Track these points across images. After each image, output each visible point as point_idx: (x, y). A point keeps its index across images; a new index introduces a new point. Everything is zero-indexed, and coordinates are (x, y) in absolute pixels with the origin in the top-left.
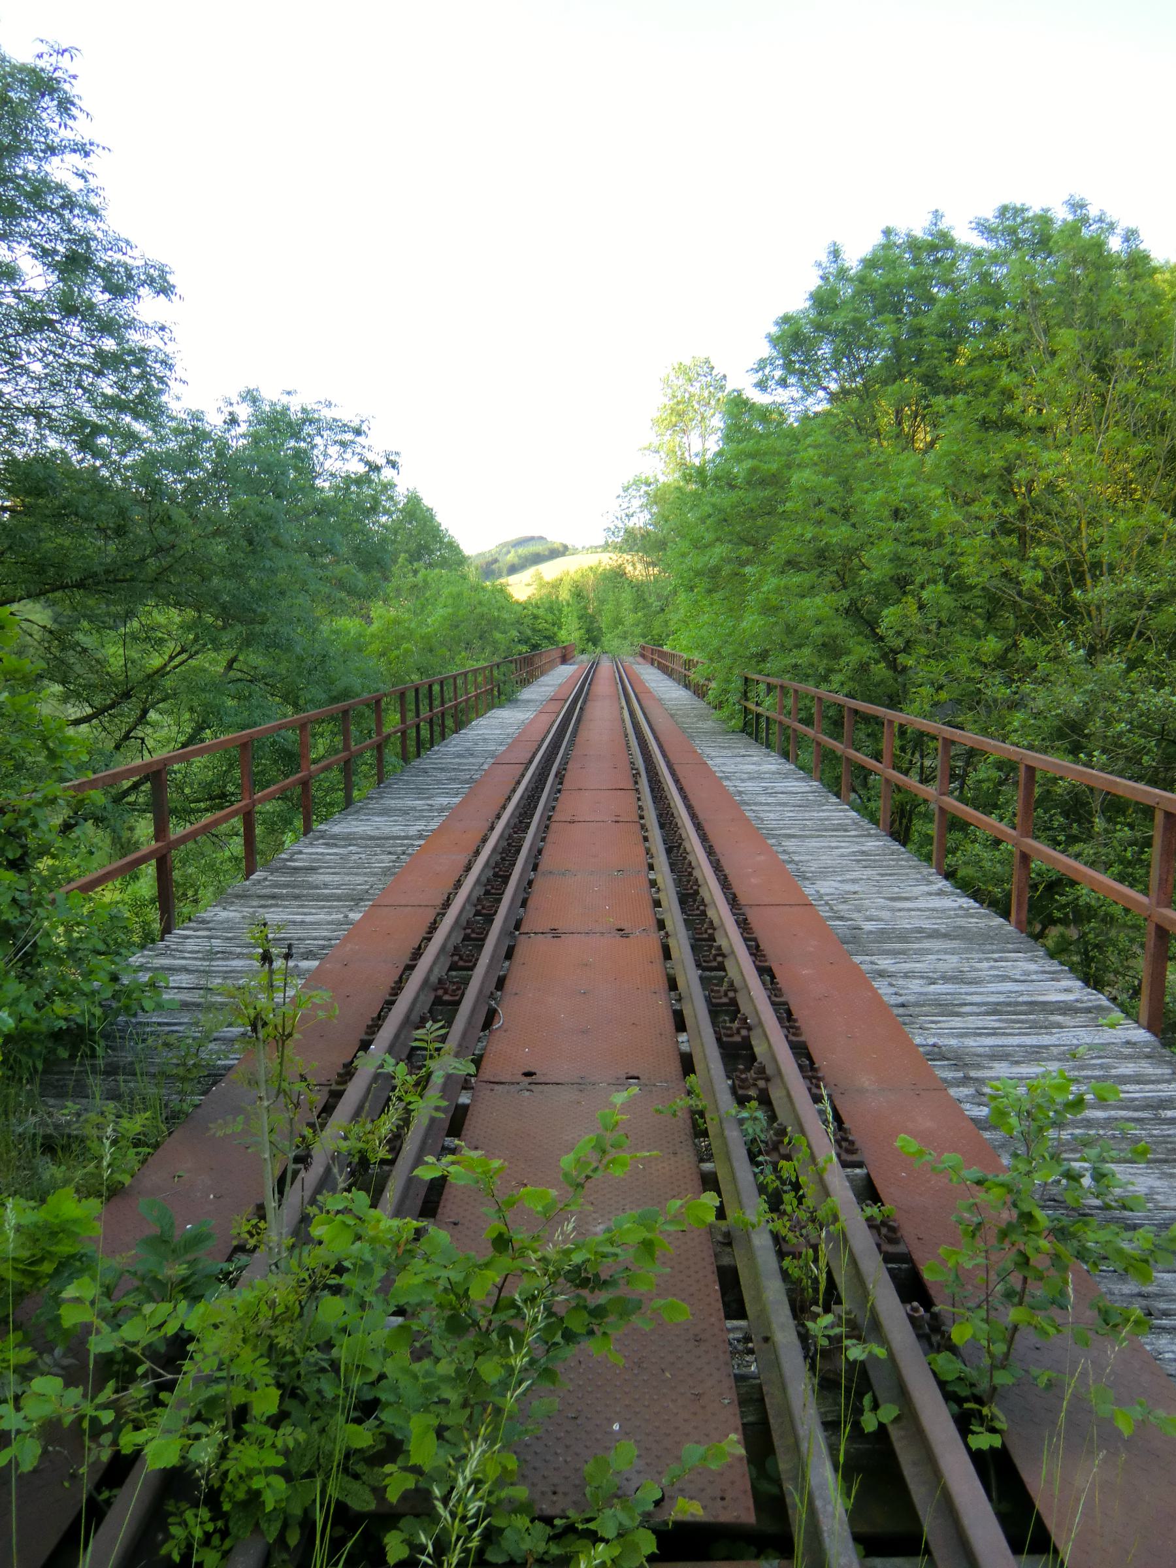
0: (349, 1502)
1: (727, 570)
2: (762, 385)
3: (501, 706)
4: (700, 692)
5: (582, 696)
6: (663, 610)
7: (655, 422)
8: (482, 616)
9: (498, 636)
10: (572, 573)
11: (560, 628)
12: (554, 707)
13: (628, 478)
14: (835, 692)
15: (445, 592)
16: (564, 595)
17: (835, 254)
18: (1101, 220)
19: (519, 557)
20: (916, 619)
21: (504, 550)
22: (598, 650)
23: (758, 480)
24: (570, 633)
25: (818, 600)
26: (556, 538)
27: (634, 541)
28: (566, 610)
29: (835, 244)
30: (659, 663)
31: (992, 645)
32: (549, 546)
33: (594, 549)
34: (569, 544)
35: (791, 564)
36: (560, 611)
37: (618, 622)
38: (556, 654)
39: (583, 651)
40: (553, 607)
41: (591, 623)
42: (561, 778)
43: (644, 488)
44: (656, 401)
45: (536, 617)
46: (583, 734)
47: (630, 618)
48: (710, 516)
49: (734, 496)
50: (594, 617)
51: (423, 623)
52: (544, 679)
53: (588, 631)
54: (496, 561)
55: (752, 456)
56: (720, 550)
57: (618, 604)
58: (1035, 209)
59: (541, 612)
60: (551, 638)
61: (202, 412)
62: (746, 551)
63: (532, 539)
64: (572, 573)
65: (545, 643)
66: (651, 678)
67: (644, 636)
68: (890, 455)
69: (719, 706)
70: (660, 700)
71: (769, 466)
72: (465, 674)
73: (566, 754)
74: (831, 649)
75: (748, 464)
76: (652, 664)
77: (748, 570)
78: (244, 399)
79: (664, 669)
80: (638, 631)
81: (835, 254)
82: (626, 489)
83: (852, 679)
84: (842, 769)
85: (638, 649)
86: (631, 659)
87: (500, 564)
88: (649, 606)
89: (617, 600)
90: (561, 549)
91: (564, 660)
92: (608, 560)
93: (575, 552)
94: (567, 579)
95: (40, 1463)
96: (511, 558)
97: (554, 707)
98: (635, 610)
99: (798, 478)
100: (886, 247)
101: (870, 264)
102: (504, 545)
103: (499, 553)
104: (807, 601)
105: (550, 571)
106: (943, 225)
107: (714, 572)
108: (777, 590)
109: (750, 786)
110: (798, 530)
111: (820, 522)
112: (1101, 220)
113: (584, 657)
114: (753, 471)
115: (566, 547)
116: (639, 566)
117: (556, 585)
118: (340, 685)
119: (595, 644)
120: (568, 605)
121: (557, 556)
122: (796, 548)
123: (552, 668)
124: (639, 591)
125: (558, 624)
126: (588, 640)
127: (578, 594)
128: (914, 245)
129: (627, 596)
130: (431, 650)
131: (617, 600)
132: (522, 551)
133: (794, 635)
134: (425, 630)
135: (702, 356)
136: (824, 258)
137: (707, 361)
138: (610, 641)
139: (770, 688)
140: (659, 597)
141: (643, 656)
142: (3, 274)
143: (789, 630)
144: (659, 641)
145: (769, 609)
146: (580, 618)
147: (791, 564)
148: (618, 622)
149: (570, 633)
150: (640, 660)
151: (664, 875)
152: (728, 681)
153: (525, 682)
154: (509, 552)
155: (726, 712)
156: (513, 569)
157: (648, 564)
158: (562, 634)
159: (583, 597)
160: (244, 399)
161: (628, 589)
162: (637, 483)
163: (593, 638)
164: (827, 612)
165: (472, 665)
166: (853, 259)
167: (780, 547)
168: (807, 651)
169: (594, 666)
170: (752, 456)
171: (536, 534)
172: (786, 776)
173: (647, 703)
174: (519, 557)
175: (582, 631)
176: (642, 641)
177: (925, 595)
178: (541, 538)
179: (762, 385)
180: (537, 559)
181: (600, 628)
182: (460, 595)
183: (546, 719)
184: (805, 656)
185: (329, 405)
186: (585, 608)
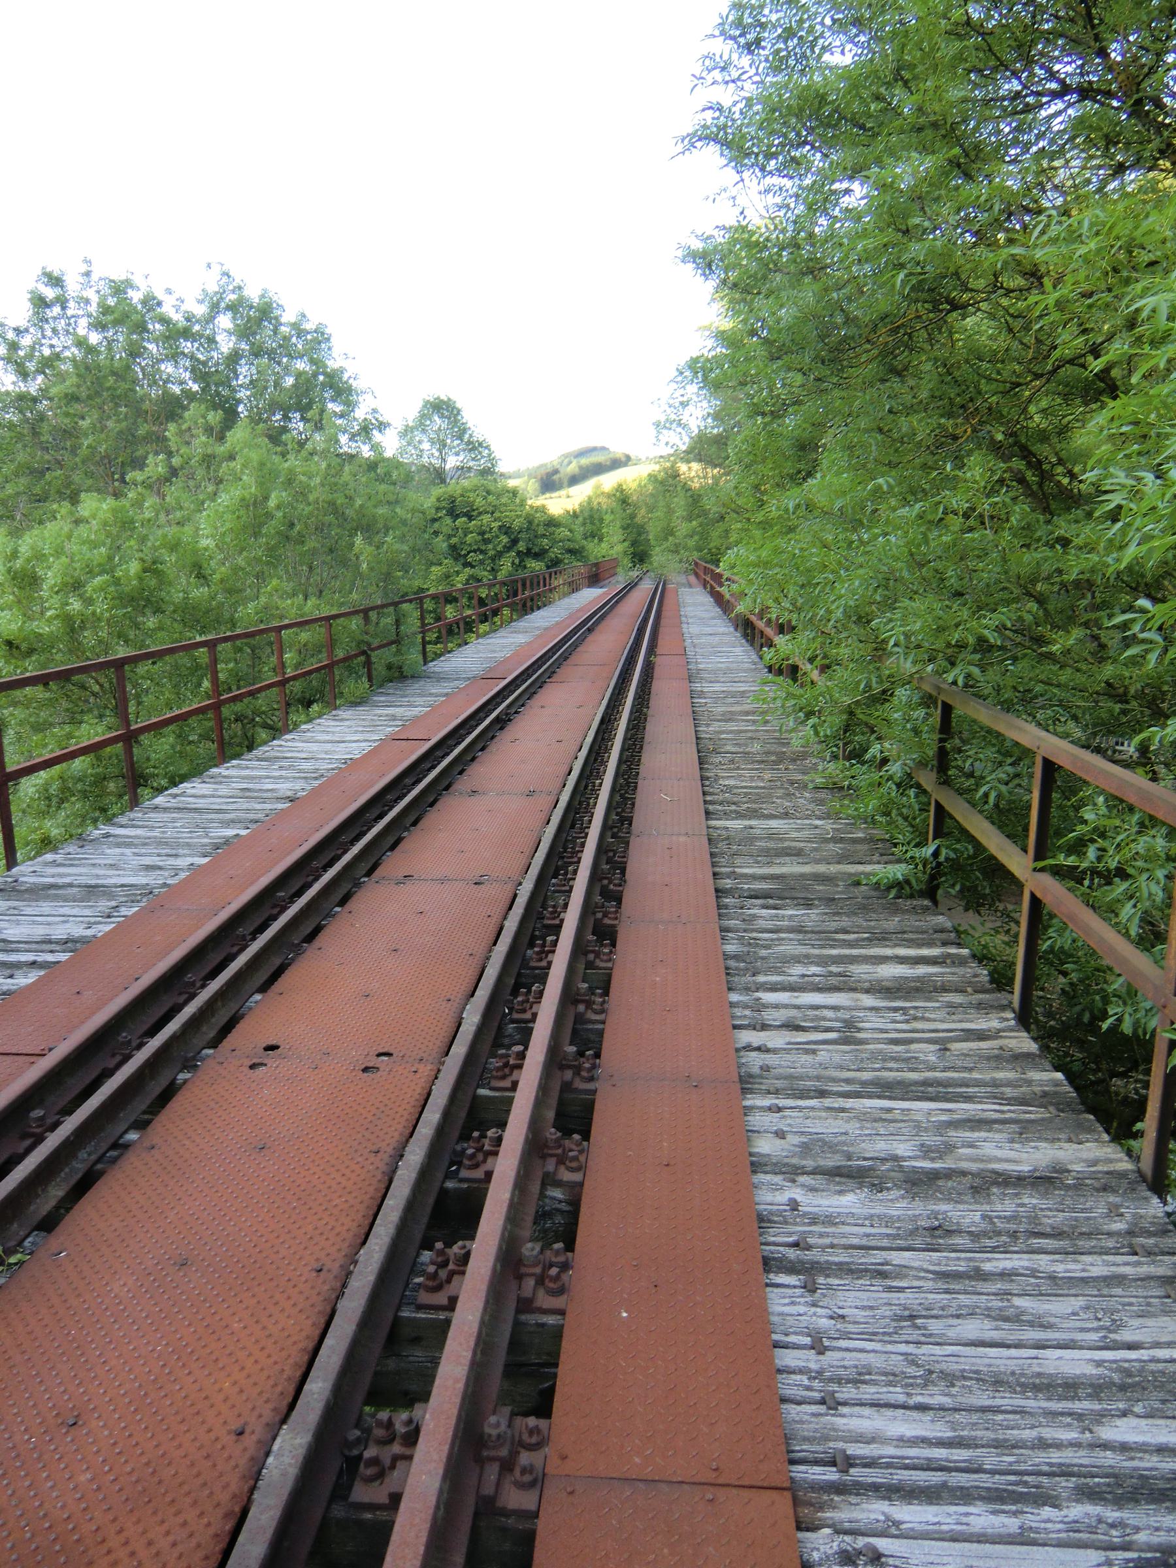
6: (722, 518)
19: (581, 468)
21: (566, 461)
26: (618, 449)
28: (608, 518)
29: (692, 256)
30: (712, 587)
32: (611, 456)
36: (601, 520)
37: (669, 532)
41: (639, 534)
47: (683, 528)
50: (642, 527)
53: (634, 544)
54: (556, 472)
57: (670, 511)
61: (620, 485)
63: (594, 449)
67: (700, 550)
76: (705, 588)
80: (691, 543)
86: (682, 579)
87: (561, 475)
89: (668, 506)
90: (623, 459)
93: (638, 462)
95: (108, 493)
96: (573, 468)
98: (689, 519)
102: (566, 456)
103: (561, 464)
105: (608, 482)
115: (628, 458)
124: (695, 499)
125: (595, 535)
129: (680, 503)
131: (668, 506)
132: (584, 461)
138: (659, 557)
141: (696, 575)
146: (624, 528)
148: (669, 532)
149: (612, 546)
150: (693, 579)
154: (570, 463)
159: (628, 504)
161: (682, 494)
171: (599, 445)
174: (581, 468)
175: (626, 544)
178: (604, 449)
186: (633, 516)
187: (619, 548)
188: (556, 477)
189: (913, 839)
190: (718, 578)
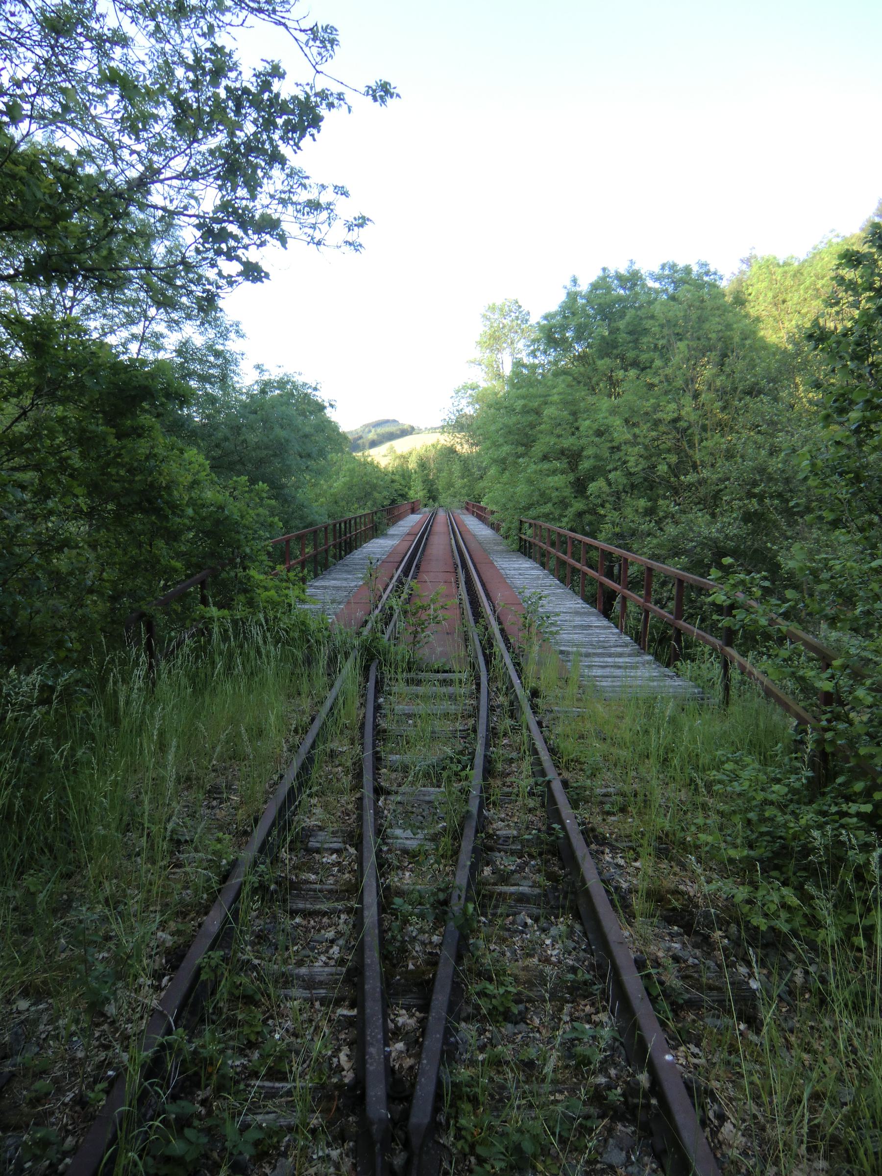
1: (511, 459)
2: (533, 354)
3: (377, 537)
4: (495, 527)
5: (427, 532)
7: (479, 343)
8: (367, 483)
9: (376, 495)
10: (418, 448)
11: (410, 489)
12: (410, 538)
13: (460, 384)
14: (562, 527)
15: (345, 468)
16: (412, 465)
17: (575, 281)
18: (715, 274)
20: (606, 488)
22: (436, 505)
23: (526, 411)
24: (417, 492)
25: (556, 478)
26: (406, 421)
27: (460, 425)
28: (414, 476)
31: (642, 503)
33: (433, 430)
35: (545, 458)
36: (410, 477)
37: (450, 485)
38: (408, 507)
39: (426, 506)
40: (405, 475)
42: (418, 567)
43: (470, 392)
44: (478, 329)
45: (393, 481)
46: (429, 551)
47: (459, 483)
49: (514, 419)
51: (331, 487)
52: (401, 523)
53: (429, 491)
54: (360, 438)
55: (523, 397)
56: (506, 449)
57: (451, 473)
58: (681, 264)
59: (397, 477)
60: (404, 496)
62: (521, 449)
63: (387, 422)
65: (399, 499)
66: (472, 524)
69: (507, 538)
70: (474, 536)
72: (355, 518)
73: (420, 558)
74: (564, 504)
75: (521, 402)
77: (521, 460)
79: (480, 518)
80: (464, 491)
81: (575, 281)
82: (457, 392)
83: (572, 520)
84: (568, 571)
85: (464, 505)
86: (459, 511)
88: (472, 474)
91: (413, 511)
92: (445, 440)
93: (420, 432)
96: (371, 436)
97: (410, 538)
98: (463, 477)
99: (549, 411)
100: (603, 279)
101: (595, 287)
102: (367, 426)
104: (550, 479)
105: (402, 446)
106: (636, 267)
107: (503, 461)
108: (535, 472)
109: (513, 572)
110: (547, 440)
111: (559, 436)
112: (715, 274)
113: (426, 509)
114: (525, 406)
115: (413, 428)
116: (466, 446)
117: (405, 458)
118: (309, 519)
119: (434, 501)
122: (546, 450)
123: (405, 516)
124: (465, 461)
126: (429, 498)
127: (423, 465)
128: (619, 277)
129: (456, 468)
130: (336, 502)
132: (381, 430)
133: (544, 498)
134: (332, 491)
135: (513, 297)
136: (569, 284)
138: (444, 499)
139: (530, 525)
140: (479, 468)
141: (467, 509)
142: (10, 227)
144: (478, 500)
145: (530, 482)
146: (424, 482)
147: (545, 458)
148: (450, 485)
149: (417, 492)
150: (465, 511)
151: (453, 542)
152: (511, 522)
153: (394, 522)
154: (370, 431)
155: (510, 540)
156: (373, 444)
157: (472, 445)
158: (411, 493)
162: (465, 388)
163: (432, 496)
164: (561, 484)
165: (361, 512)
166: (584, 287)
167: (538, 449)
168: (550, 505)
169: (434, 515)
170: (523, 397)
171: (391, 418)
172: (533, 569)
173: (467, 537)
176: (466, 499)
177: (611, 476)
178: (394, 421)
179: (533, 354)
180: (391, 437)
182: (354, 469)
183: (406, 544)
184: (548, 508)
185: (300, 374)
186: (427, 475)
187: (421, 494)
188: (360, 442)
189: (622, 745)
190: (483, 509)
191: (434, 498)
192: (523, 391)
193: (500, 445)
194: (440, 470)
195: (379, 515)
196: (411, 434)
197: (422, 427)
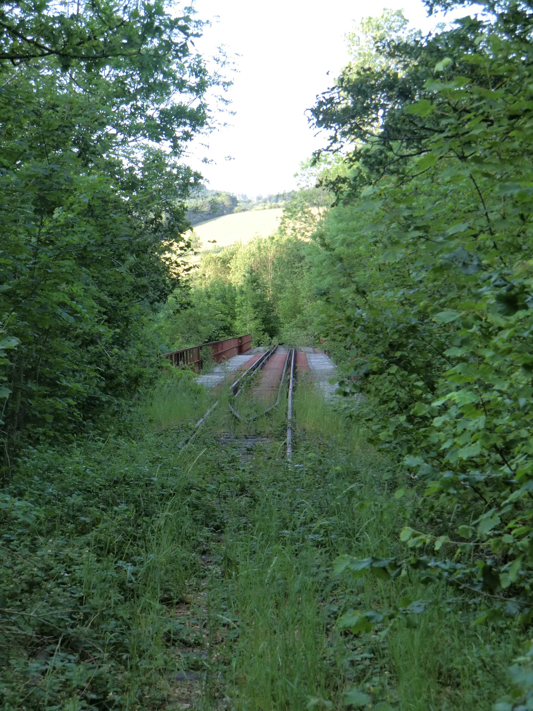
0: (486, 90)
11: (234, 318)
27: (230, 284)
28: (239, 298)
34: (237, 193)
36: (233, 299)
37: (296, 311)
38: (234, 344)
41: (268, 312)
48: (324, 260)
53: (265, 321)
56: (329, 280)
60: (227, 329)
64: (245, 242)
68: (379, 440)
71: (352, 238)
78: (507, 94)
90: (227, 203)
91: (241, 351)
94: (243, 252)
115: (234, 201)
120: (242, 292)
121: (222, 214)
137: (399, 13)
143: (391, 345)
146: (255, 307)
148: (296, 311)
160: (507, 94)
170: (344, 231)
175: (258, 321)
181: (277, 318)
186: (262, 297)
187: (251, 325)
191: (272, 332)
192: (342, 225)
193: (107, 402)
194: (280, 289)
195: (204, 350)
196: (230, 211)
197: (252, 196)
